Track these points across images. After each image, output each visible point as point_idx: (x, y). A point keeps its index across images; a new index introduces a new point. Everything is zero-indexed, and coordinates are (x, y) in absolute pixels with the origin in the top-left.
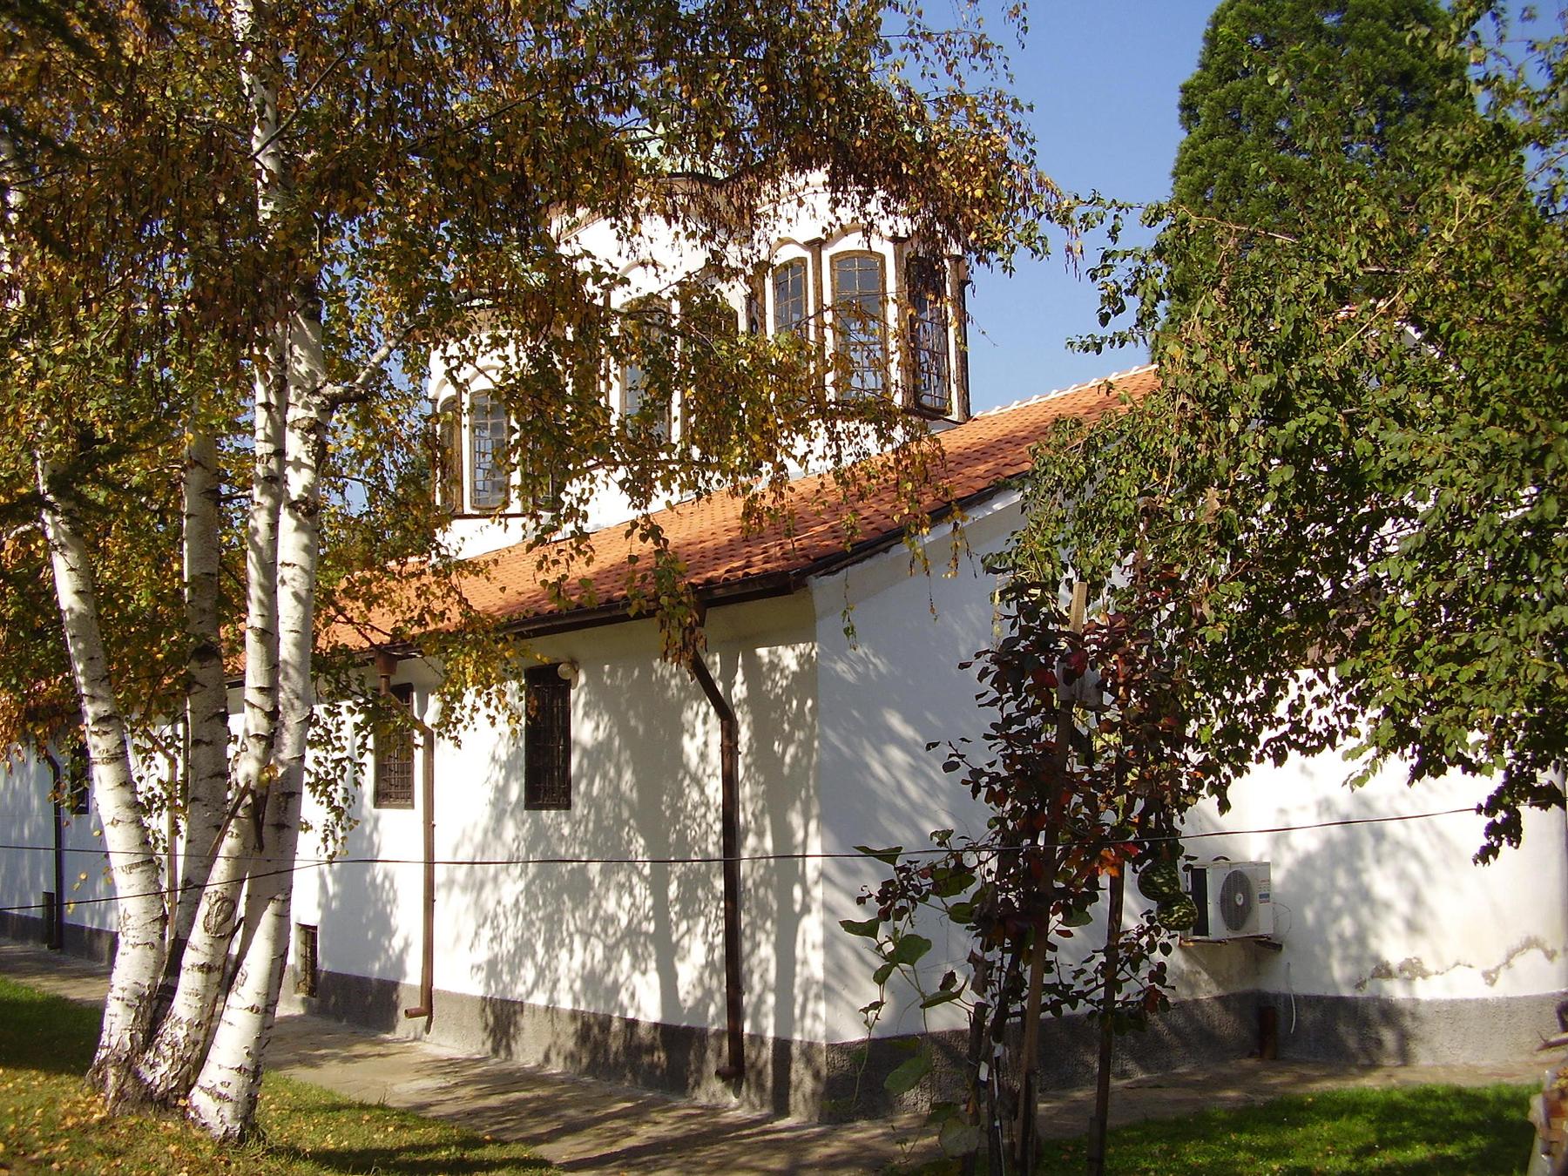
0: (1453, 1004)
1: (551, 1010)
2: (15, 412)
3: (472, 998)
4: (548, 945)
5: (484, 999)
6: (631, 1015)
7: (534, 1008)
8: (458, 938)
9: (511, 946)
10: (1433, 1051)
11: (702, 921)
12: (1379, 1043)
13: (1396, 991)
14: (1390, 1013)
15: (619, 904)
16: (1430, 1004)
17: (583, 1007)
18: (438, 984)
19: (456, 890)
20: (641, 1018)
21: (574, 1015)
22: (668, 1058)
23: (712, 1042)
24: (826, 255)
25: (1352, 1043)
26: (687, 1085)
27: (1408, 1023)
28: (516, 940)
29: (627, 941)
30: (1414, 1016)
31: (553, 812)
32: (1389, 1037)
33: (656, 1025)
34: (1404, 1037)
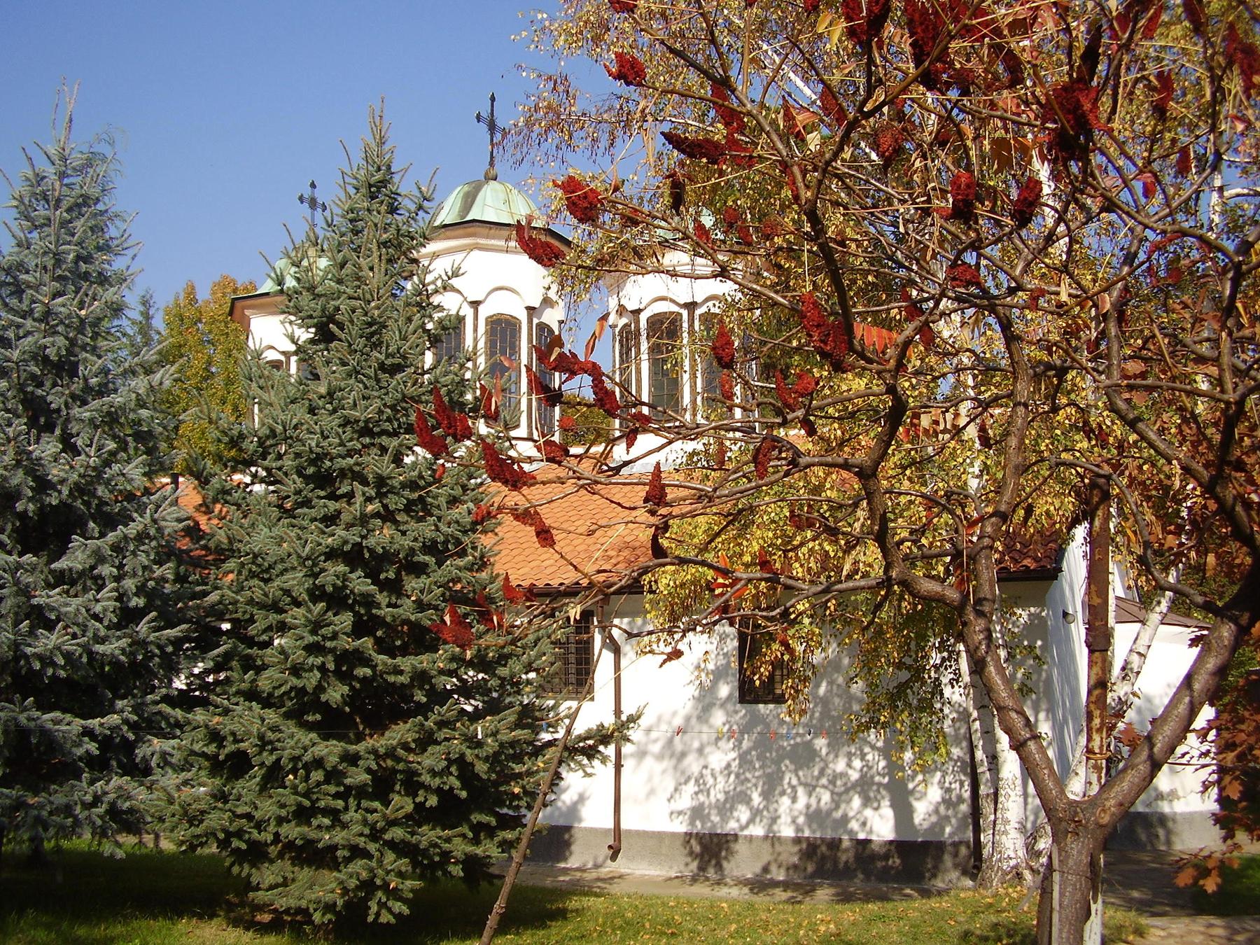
0: (1191, 814)
1: (772, 839)
2: (1052, 504)
3: (673, 835)
4: (767, 795)
5: (689, 835)
6: (861, 836)
7: (751, 839)
8: (652, 792)
9: (721, 797)
10: (1183, 841)
11: (938, 774)
12: (1157, 836)
13: (1165, 807)
14: (1163, 819)
15: (849, 765)
16: (1181, 814)
17: (807, 833)
18: (624, 826)
19: (649, 762)
20: (874, 838)
21: (797, 840)
22: (903, 861)
23: (949, 848)
24: (698, 312)
25: (1143, 837)
26: (924, 877)
27: (1170, 824)
28: (726, 793)
29: (859, 789)
30: (1174, 821)
31: (771, 706)
32: (1161, 832)
33: (891, 842)
34: (1169, 832)
